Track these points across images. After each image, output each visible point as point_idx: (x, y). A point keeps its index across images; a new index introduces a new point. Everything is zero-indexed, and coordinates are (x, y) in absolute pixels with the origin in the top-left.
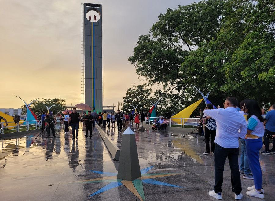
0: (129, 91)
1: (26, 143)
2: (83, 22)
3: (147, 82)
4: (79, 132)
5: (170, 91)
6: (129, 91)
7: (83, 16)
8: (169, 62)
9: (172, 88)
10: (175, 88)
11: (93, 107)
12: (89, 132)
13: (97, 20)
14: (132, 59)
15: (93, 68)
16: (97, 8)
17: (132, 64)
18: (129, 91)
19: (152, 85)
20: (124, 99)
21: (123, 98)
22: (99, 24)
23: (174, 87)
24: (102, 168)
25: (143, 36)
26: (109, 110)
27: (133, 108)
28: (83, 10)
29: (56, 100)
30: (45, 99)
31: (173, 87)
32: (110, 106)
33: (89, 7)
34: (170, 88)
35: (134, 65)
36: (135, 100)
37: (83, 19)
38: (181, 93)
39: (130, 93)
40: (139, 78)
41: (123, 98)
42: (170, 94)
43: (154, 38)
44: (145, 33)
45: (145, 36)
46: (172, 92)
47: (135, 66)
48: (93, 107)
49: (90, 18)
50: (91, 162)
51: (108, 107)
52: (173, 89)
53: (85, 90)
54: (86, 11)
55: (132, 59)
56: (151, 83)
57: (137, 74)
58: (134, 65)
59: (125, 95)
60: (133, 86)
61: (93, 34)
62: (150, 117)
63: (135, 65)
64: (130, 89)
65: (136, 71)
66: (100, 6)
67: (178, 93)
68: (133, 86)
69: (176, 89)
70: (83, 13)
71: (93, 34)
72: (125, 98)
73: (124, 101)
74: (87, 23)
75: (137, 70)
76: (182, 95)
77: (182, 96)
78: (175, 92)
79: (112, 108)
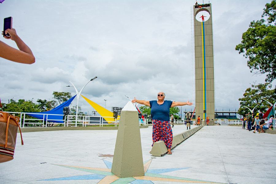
2: (193, 24)
3: (265, 76)
6: (247, 92)
7: (193, 18)
11: (204, 110)
14: (240, 49)
15: (203, 69)
16: (206, 7)
19: (271, 80)
20: (241, 101)
21: (240, 100)
28: (193, 13)
33: (199, 7)
35: (244, 56)
36: (255, 102)
37: (193, 21)
40: (251, 72)
41: (240, 100)
43: (269, 22)
44: (258, 19)
45: (257, 22)
50: (229, 176)
55: (240, 49)
56: (270, 79)
58: (244, 56)
59: (242, 97)
60: (253, 86)
63: (245, 55)
64: (249, 90)
65: (247, 64)
70: (193, 16)
71: (203, 34)
73: (241, 103)
79: (234, 114)
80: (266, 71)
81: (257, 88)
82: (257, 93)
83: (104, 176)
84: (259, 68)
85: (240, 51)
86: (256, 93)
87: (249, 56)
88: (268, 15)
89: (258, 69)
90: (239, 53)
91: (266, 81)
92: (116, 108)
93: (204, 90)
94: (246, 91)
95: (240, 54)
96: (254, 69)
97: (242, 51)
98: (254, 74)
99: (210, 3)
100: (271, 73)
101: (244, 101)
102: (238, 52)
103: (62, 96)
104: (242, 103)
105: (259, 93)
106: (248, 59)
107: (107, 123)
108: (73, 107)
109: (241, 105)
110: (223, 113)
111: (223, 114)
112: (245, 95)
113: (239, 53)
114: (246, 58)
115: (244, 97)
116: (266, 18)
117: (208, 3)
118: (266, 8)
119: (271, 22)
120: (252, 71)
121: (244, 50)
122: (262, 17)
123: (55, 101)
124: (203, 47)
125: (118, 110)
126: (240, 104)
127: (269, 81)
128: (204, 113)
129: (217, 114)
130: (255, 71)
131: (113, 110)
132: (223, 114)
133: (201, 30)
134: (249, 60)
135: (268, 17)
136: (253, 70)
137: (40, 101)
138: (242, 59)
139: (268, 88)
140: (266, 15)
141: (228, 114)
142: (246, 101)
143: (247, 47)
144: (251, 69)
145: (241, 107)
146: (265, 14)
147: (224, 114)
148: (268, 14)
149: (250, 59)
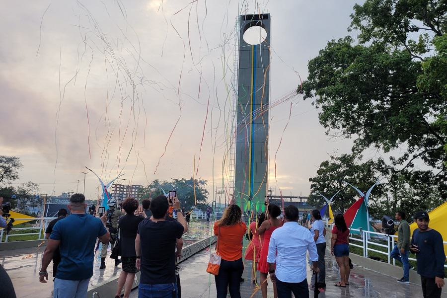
0: (323, 167)
2: (237, 47)
5: (405, 163)
6: (323, 167)
7: (238, 38)
9: (411, 156)
10: (420, 155)
14: (305, 89)
16: (260, 20)
17: (305, 98)
19: (362, 150)
20: (312, 183)
21: (310, 180)
22: (264, 48)
23: (416, 152)
24: (429, 219)
25: (336, 42)
26: (293, 202)
27: (325, 201)
29: (192, 182)
30: (176, 180)
31: (413, 154)
32: (304, 196)
33: (249, 21)
34: (406, 155)
37: (238, 43)
38: (438, 168)
40: (327, 134)
41: (310, 180)
42: (410, 169)
46: (412, 166)
47: (315, 106)
52: (415, 157)
53: (236, 164)
54: (244, 28)
55: (305, 89)
56: (360, 146)
57: (323, 126)
58: (313, 104)
59: (315, 175)
60: (332, 157)
61: (254, 65)
64: (325, 164)
66: (266, 17)
67: (430, 168)
68: (332, 157)
69: (422, 158)
71: (254, 65)
73: (312, 186)
74: (245, 50)
75: (324, 119)
76: (441, 174)
77: (441, 177)
78: (421, 166)
80: (353, 132)
81: (338, 162)
82: (340, 170)
84: (341, 126)
85: (305, 95)
86: (337, 170)
87: (321, 105)
88: (359, 28)
89: (339, 128)
90: (304, 99)
91: (353, 150)
92: (120, 185)
93: (250, 161)
94: (321, 167)
96: (331, 129)
97: (308, 95)
99: (268, 13)
100: (362, 137)
101: (319, 182)
102: (302, 96)
104: (315, 185)
105: (341, 170)
106: (321, 110)
109: (313, 189)
110: (291, 198)
112: (319, 172)
113: (304, 99)
114: (317, 107)
116: (356, 33)
117: (262, 11)
118: (354, 12)
119: (364, 42)
121: (313, 92)
122: (349, 30)
125: (124, 188)
127: (357, 150)
130: (333, 131)
131: (114, 189)
133: (250, 59)
134: (322, 112)
135: (359, 32)
138: (310, 109)
139: (357, 162)
140: (356, 28)
141: (299, 199)
142: (320, 182)
143: (319, 87)
145: (311, 193)
146: (354, 26)
147: (292, 199)
148: (360, 25)
149: (324, 110)
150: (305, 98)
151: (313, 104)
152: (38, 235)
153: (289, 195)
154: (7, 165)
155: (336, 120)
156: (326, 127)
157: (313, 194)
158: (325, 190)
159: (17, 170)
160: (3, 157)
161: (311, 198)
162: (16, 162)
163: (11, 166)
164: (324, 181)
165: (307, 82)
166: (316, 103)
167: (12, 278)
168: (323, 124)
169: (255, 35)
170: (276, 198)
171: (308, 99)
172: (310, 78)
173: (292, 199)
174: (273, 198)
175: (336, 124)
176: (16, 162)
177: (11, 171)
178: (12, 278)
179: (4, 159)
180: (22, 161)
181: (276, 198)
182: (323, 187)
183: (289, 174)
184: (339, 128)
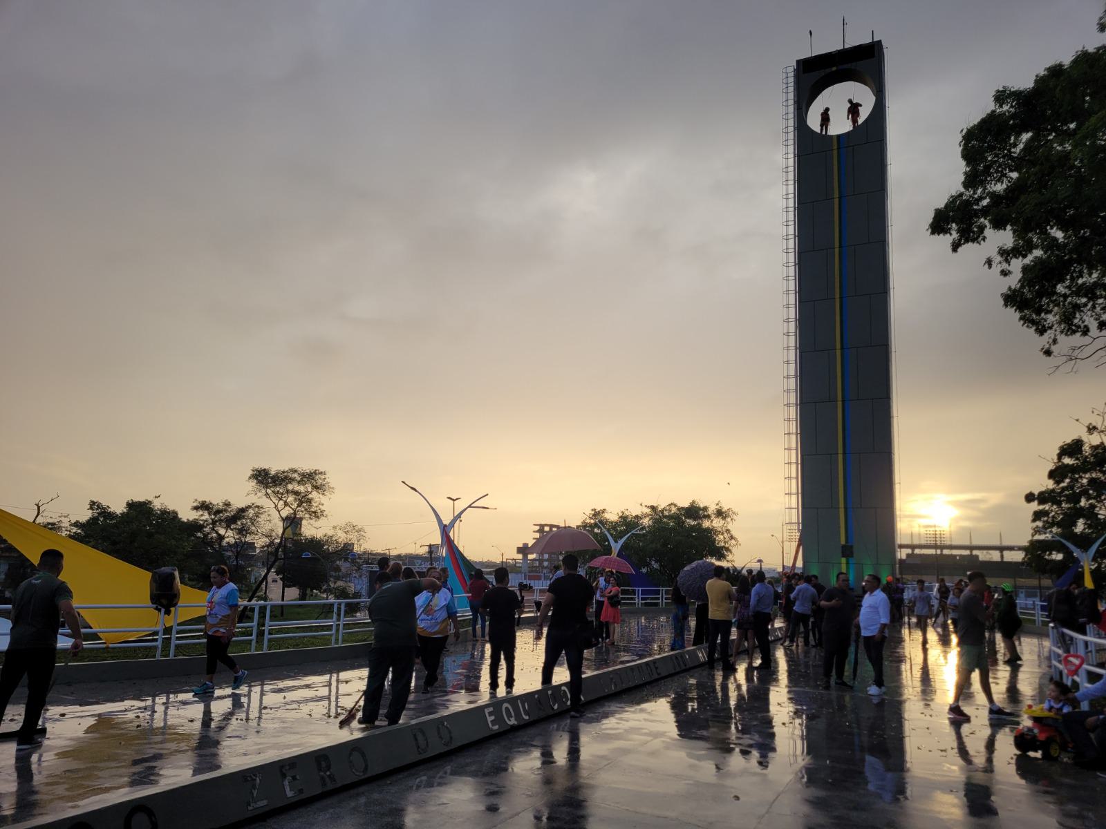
0: (1067, 461)
1: (9, 636)
4: (860, 647)
6: (1067, 461)
8: (1087, 98)
12: (503, 663)
13: (864, 114)
16: (862, 63)
17: (955, 247)
18: (1070, 456)
20: (1035, 506)
21: (1030, 498)
22: (870, 137)
33: (815, 74)
39: (1072, 469)
40: (1048, 353)
41: (1030, 498)
47: (996, 269)
48: (843, 542)
49: (825, 118)
51: (1002, 549)
60: (1091, 429)
62: (685, 648)
64: (1073, 448)
72: (1043, 498)
73: (1037, 516)
74: (813, 151)
83: (606, 762)
85: (955, 235)
89: (1086, 331)
95: (960, 249)
96: (1062, 338)
97: (969, 234)
98: (1065, 358)
101: (1059, 503)
103: (290, 487)
107: (95, 637)
108: (335, 527)
109: (1039, 524)
111: (1002, 556)
112: (1056, 474)
115: (1050, 484)
120: (1053, 348)
123: (258, 507)
124: (837, 250)
126: (1030, 517)
128: (844, 560)
129: (975, 552)
132: (1002, 556)
136: (1055, 341)
137: (204, 506)
144: (1049, 335)
150: (955, 247)
151: (989, 262)
152: (331, 635)
153: (997, 543)
154: (301, 489)
155: (1077, 307)
156: (1042, 331)
157: (1101, 548)
158: (1080, 526)
159: (323, 499)
160: (296, 471)
161: (1035, 550)
162: (320, 482)
163: (310, 490)
164: (1075, 499)
165: (961, 195)
166: (999, 259)
167: (1011, 744)
168: (1033, 322)
169: (837, 107)
170: (955, 552)
171: (968, 248)
172: (972, 180)
173: (1006, 553)
174: (946, 552)
175: (1076, 321)
176: (320, 482)
177: (309, 501)
178: (1011, 744)
179: (295, 475)
180: (331, 479)
181: (955, 552)
182: (1067, 522)
183: (955, 489)
184: (1086, 331)
